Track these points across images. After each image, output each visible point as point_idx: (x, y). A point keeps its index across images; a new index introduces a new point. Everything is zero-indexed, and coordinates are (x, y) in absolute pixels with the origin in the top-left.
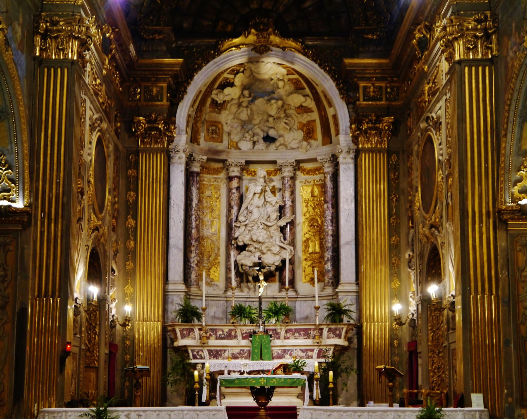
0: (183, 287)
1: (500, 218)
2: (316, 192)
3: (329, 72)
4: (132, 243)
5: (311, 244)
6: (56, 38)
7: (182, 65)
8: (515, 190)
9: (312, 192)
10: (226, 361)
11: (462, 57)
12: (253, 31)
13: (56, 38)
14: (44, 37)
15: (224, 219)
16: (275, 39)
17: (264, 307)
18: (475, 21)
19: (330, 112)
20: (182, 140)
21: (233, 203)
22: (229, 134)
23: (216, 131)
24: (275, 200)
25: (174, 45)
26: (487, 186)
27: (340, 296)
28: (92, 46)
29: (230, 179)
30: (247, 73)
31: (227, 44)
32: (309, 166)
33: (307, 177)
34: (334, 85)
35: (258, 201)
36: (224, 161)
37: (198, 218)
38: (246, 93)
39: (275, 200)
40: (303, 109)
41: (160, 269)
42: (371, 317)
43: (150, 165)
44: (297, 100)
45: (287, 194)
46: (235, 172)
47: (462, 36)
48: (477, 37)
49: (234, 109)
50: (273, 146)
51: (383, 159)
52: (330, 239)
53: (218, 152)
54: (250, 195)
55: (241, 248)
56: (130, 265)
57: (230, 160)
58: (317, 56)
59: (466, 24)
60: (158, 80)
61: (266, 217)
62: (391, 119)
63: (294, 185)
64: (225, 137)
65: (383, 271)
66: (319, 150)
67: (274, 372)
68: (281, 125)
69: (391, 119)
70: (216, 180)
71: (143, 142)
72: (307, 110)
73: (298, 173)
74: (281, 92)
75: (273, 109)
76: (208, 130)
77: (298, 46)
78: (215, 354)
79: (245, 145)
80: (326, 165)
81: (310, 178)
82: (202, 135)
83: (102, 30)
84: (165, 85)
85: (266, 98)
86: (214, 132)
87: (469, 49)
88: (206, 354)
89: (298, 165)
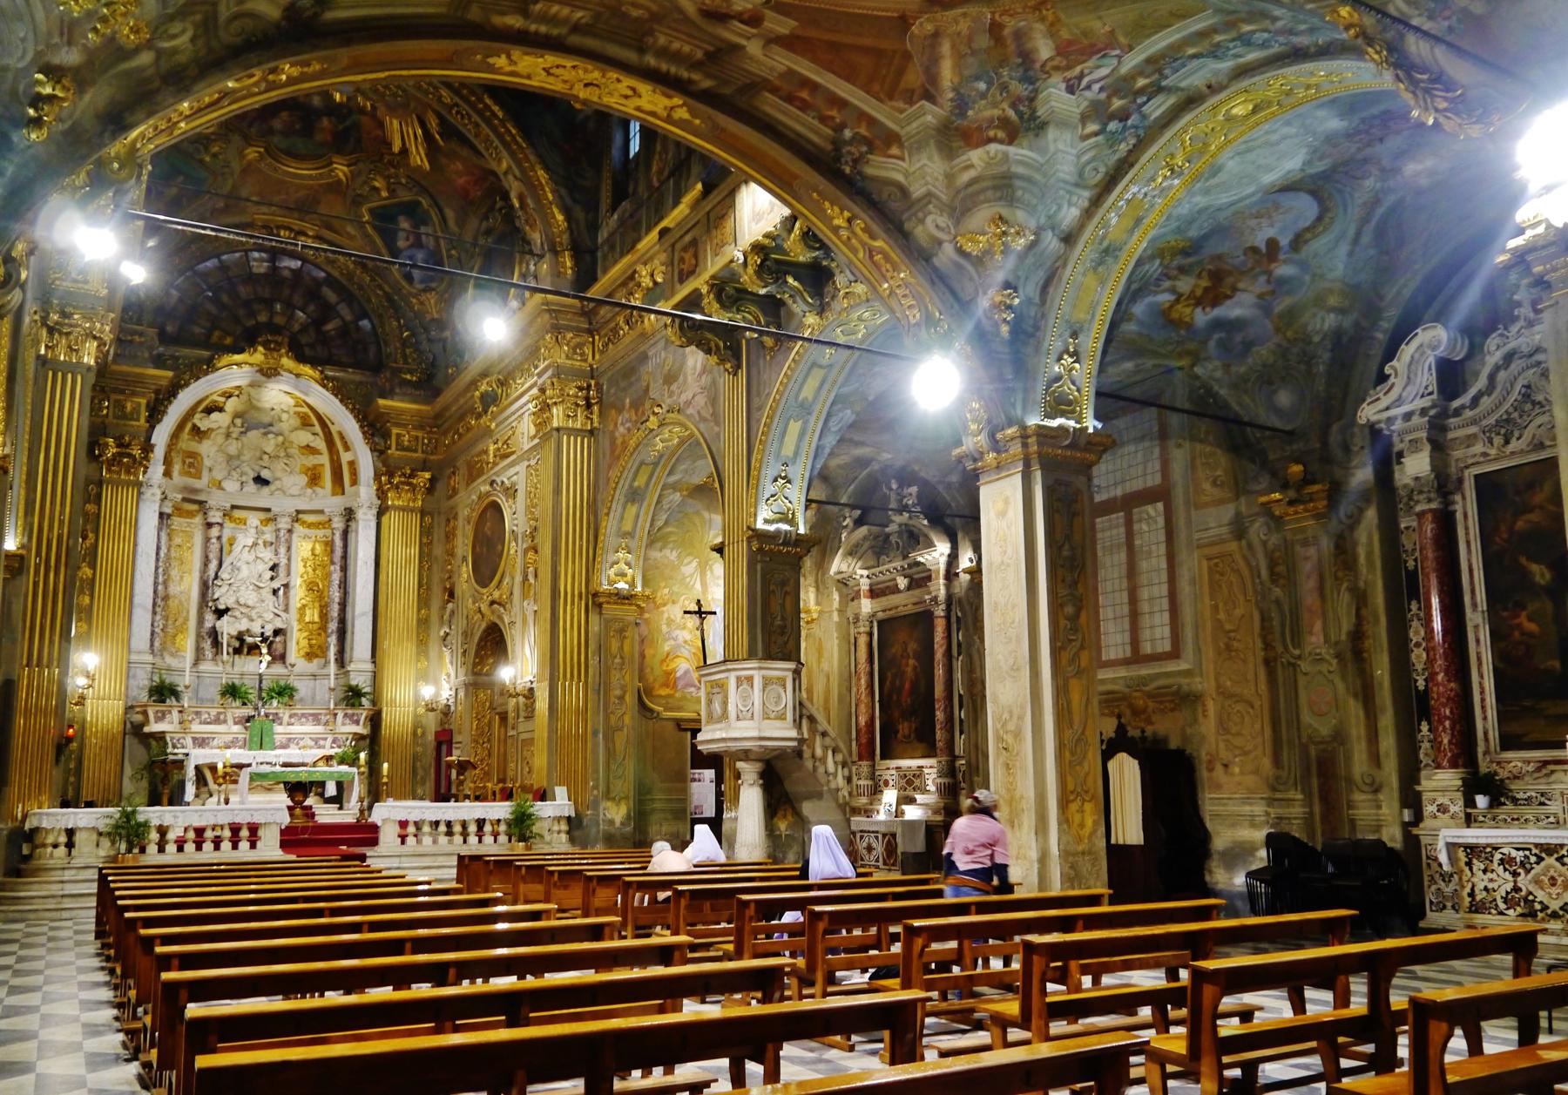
1: (595, 600)
3: (352, 411)
4: (87, 600)
5: (308, 612)
6: (68, 334)
8: (612, 572)
9: (313, 550)
10: (217, 751)
12: (260, 348)
14: (51, 331)
15: (196, 576)
16: (287, 362)
17: (265, 685)
19: (345, 457)
21: (211, 556)
23: (193, 463)
24: (267, 555)
26: (580, 566)
29: (209, 525)
30: (244, 398)
31: (227, 359)
32: (310, 518)
33: (307, 531)
34: (357, 426)
35: (246, 556)
36: (201, 503)
38: (238, 421)
39: (267, 555)
40: (310, 450)
42: (393, 701)
44: (304, 437)
45: (282, 550)
46: (215, 517)
49: (220, 439)
50: (266, 490)
51: (415, 519)
52: (336, 607)
53: (195, 491)
54: (237, 548)
55: (220, 613)
57: (211, 503)
60: (134, 394)
62: (427, 475)
64: (205, 473)
65: (410, 648)
66: (328, 501)
67: (315, 764)
68: (279, 466)
69: (427, 475)
70: (189, 525)
71: (109, 470)
74: (285, 426)
75: (270, 445)
77: (317, 375)
78: (201, 742)
80: (336, 519)
82: (177, 468)
84: (143, 401)
86: (191, 465)
88: (189, 741)
89: (297, 516)
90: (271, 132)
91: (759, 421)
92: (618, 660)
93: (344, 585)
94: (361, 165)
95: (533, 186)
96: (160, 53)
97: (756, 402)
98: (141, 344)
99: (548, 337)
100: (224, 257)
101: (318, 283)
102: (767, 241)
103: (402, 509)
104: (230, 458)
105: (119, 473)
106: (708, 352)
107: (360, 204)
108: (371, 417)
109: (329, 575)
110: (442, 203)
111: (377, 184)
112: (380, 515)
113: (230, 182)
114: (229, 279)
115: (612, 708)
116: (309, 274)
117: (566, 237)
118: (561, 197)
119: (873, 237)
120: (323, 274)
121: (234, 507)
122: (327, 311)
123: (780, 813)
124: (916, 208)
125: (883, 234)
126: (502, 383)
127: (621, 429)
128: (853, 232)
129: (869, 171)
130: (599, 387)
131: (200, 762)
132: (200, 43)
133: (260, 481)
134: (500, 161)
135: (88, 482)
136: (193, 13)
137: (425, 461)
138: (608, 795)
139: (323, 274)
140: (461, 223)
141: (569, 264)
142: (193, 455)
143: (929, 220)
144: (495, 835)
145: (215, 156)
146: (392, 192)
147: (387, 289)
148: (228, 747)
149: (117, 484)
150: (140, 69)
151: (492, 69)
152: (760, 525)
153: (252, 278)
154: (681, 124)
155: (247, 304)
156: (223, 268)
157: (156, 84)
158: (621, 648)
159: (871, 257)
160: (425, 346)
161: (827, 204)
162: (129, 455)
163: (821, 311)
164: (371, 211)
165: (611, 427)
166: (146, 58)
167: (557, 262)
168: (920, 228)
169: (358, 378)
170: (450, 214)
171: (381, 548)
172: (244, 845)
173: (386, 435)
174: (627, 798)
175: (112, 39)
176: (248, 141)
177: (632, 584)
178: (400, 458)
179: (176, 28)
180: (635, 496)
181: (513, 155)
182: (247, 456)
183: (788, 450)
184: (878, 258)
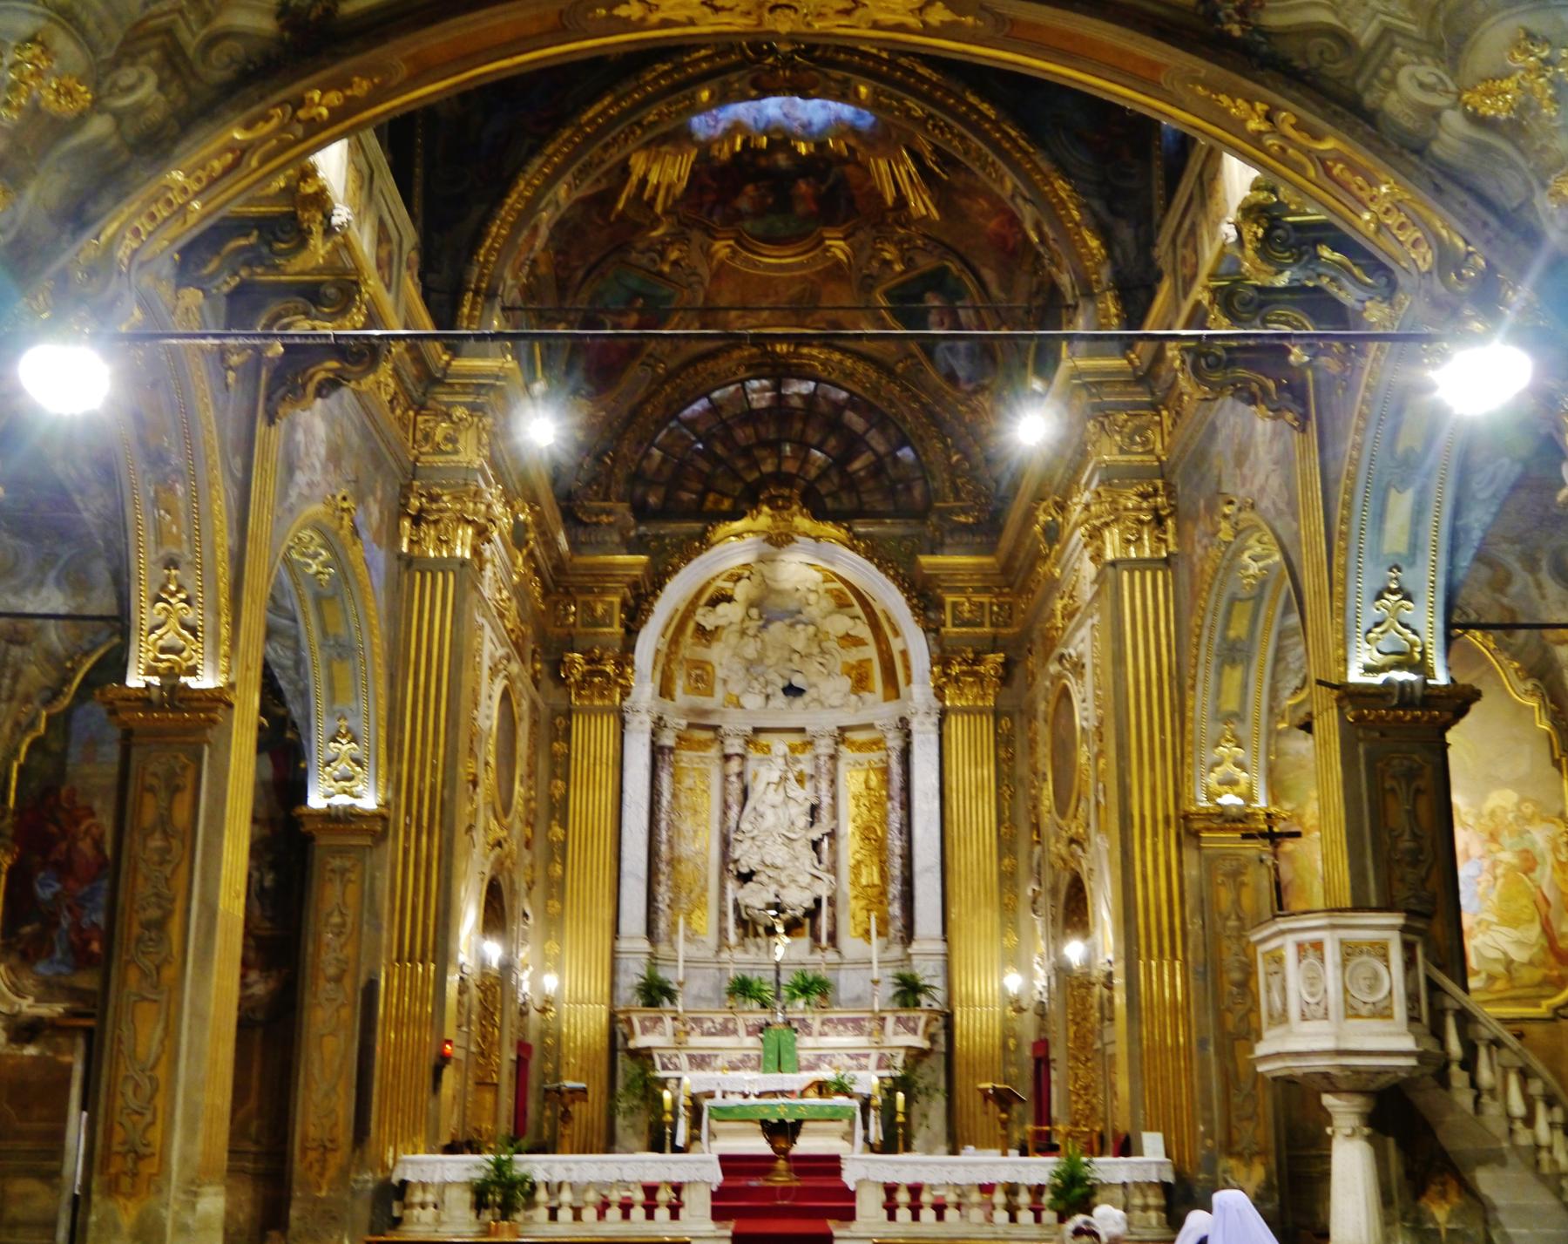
0: (645, 945)
2: (874, 782)
3: (894, 579)
4: (558, 869)
5: (864, 871)
6: (436, 522)
7: (647, 567)
8: (1212, 779)
9: (867, 782)
10: (719, 1074)
12: (766, 509)
14: (417, 520)
16: (803, 523)
17: (784, 980)
19: (896, 645)
20: (644, 690)
21: (731, 800)
22: (725, 682)
23: (702, 677)
25: (632, 533)
27: (916, 960)
29: (727, 758)
30: (756, 579)
33: (858, 755)
36: (715, 728)
37: (671, 825)
38: (754, 612)
39: (803, 795)
40: (850, 640)
41: (606, 914)
43: (591, 735)
44: (840, 624)
45: (824, 785)
46: (734, 746)
47: (1116, 520)
48: (1141, 522)
50: (799, 702)
51: (986, 726)
53: (705, 713)
55: (745, 878)
56: (555, 905)
58: (875, 552)
59: (1122, 501)
60: (604, 591)
61: (787, 823)
62: (1000, 658)
63: (836, 768)
64: (719, 690)
66: (877, 709)
67: (803, 1094)
69: (1000, 658)
71: (578, 695)
72: (858, 642)
73: (842, 748)
74: (813, 612)
75: (800, 639)
76: (689, 675)
77: (842, 534)
79: (753, 701)
80: (890, 735)
81: (863, 757)
82: (680, 685)
84: (616, 600)
85: (788, 621)
86: (699, 679)
87: (1129, 541)
88: (683, 1061)
89: (842, 735)
90: (739, 215)
92: (1232, 923)
93: (907, 828)
94: (861, 235)
95: (1052, 207)
96: (118, 116)
98: (610, 525)
100: (716, 395)
101: (839, 407)
102: (1262, 196)
103: (966, 711)
104: (750, 665)
105: (590, 698)
107: (871, 288)
108: (918, 585)
109: (885, 816)
110: (976, 263)
111: (888, 256)
112: (941, 722)
114: (723, 422)
115: (1227, 1001)
116: (825, 397)
117: (1105, 273)
118: (1094, 214)
119: (1317, 136)
120: (844, 395)
121: (757, 731)
122: (853, 444)
123: (1434, 1189)
124: (1375, 61)
125: (1327, 127)
126: (1062, 507)
128: (1285, 137)
129: (1272, 20)
131: (695, 1091)
132: (174, 89)
133: (792, 691)
134: (1001, 180)
135: (555, 713)
136: (144, 52)
137: (995, 638)
138: (1229, 1148)
139: (844, 395)
140: (1007, 287)
141: (1113, 310)
142: (701, 665)
143: (1403, 77)
144: (1037, 1214)
145: (676, 263)
146: (909, 263)
147: (925, 398)
148: (734, 1068)
149: (590, 712)
150: (99, 143)
152: (1355, 676)
153: (752, 416)
154: (943, 31)
155: (746, 452)
156: (715, 408)
157: (124, 157)
158: (1237, 902)
159: (1328, 172)
161: (1225, 100)
162: (603, 673)
164: (887, 294)
166: (99, 126)
168: (1393, 96)
169: (899, 530)
170: (988, 275)
171: (950, 772)
172: (662, 1213)
173: (940, 606)
174: (1262, 1153)
175: (36, 110)
176: (712, 234)
177: (1249, 797)
178: (960, 636)
179: (127, 76)
180: (1234, 654)
181: (1015, 167)
182: (772, 658)
183: (1396, 535)
184: (1338, 169)
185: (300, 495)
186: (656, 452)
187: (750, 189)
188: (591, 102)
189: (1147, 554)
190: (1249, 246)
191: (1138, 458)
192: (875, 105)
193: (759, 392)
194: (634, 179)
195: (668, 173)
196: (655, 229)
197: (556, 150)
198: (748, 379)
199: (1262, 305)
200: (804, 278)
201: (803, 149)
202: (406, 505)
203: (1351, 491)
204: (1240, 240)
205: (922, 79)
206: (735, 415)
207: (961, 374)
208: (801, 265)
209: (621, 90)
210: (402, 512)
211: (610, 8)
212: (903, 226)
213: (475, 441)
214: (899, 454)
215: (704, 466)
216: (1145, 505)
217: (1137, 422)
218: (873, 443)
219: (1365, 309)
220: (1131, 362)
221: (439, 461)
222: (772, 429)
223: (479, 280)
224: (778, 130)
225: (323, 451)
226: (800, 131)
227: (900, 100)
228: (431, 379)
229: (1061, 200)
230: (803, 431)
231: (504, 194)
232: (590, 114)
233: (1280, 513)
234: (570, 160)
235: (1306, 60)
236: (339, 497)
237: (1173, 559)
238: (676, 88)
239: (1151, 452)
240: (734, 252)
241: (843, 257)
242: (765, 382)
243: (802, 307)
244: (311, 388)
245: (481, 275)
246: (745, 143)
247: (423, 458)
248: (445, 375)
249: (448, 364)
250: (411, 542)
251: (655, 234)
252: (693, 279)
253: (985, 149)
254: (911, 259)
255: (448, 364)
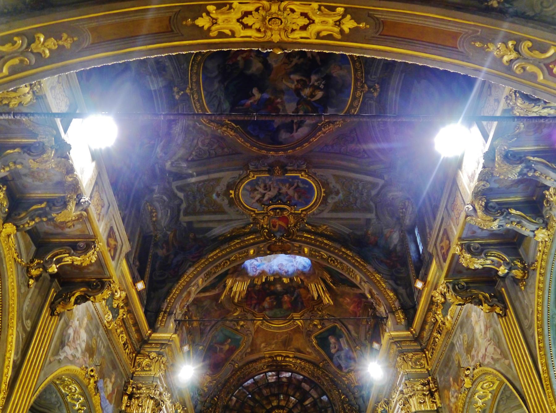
6: (138, 398)
11: (417, 409)
13: (138, 398)
14: (131, 397)
18: (422, 384)
28: (164, 407)
48: (424, 395)
83: (175, 406)
87: (421, 403)
90: (264, 309)
91: (533, 335)
95: (375, 283)
97: (526, 323)
99: (398, 359)
100: (256, 377)
101: (300, 382)
106: (480, 303)
111: (315, 323)
113: (251, 338)
114: (258, 387)
116: (295, 378)
117: (397, 304)
119: (544, 51)
120: (301, 377)
122: (305, 395)
126: (387, 403)
127: (453, 400)
130: (435, 382)
139: (301, 377)
141: (402, 317)
145: (242, 326)
146: (323, 325)
147: (330, 376)
151: (204, 33)
153: (269, 385)
155: (267, 398)
160: (354, 402)
163: (546, 225)
164: (316, 337)
165: (447, 402)
167: (395, 317)
170: (350, 327)
181: (361, 271)
185: (66, 358)
186: (234, 398)
187: (268, 299)
188: (212, 251)
189: (429, 409)
190: (478, 211)
191: (419, 370)
192: (310, 256)
193: (271, 377)
194: (228, 288)
195: (239, 287)
196: (235, 313)
197: (199, 266)
198: (268, 372)
199: (482, 251)
200: (287, 332)
201: (285, 280)
202: (126, 390)
203: (541, 327)
204: (474, 209)
205: (326, 244)
206: (263, 385)
207: (343, 366)
208: (286, 328)
209: (222, 248)
210: (124, 393)
211: (195, 18)
212: (320, 311)
213: (158, 367)
214: (322, 398)
215: (251, 403)
216: (425, 388)
217: (416, 357)
218: (313, 394)
219: (535, 235)
220: (412, 332)
221: (143, 374)
222: (276, 390)
223: (166, 308)
224: (278, 274)
225: (84, 345)
226: (285, 274)
227: (319, 252)
228: (144, 341)
229: (378, 280)
230: (287, 390)
231: (179, 279)
232: (212, 255)
233: (496, 361)
234: (203, 269)
235: (533, 10)
236: (90, 369)
237: (440, 410)
238: (241, 248)
239: (424, 368)
240: (263, 323)
241: (300, 324)
242: (273, 373)
243: (286, 344)
244: (73, 299)
245: (167, 306)
246: (266, 279)
247: (136, 373)
248: (149, 339)
249: (150, 335)
250: (127, 406)
251: (235, 314)
252: (248, 332)
253: (350, 266)
254: (323, 324)
255: (150, 335)
